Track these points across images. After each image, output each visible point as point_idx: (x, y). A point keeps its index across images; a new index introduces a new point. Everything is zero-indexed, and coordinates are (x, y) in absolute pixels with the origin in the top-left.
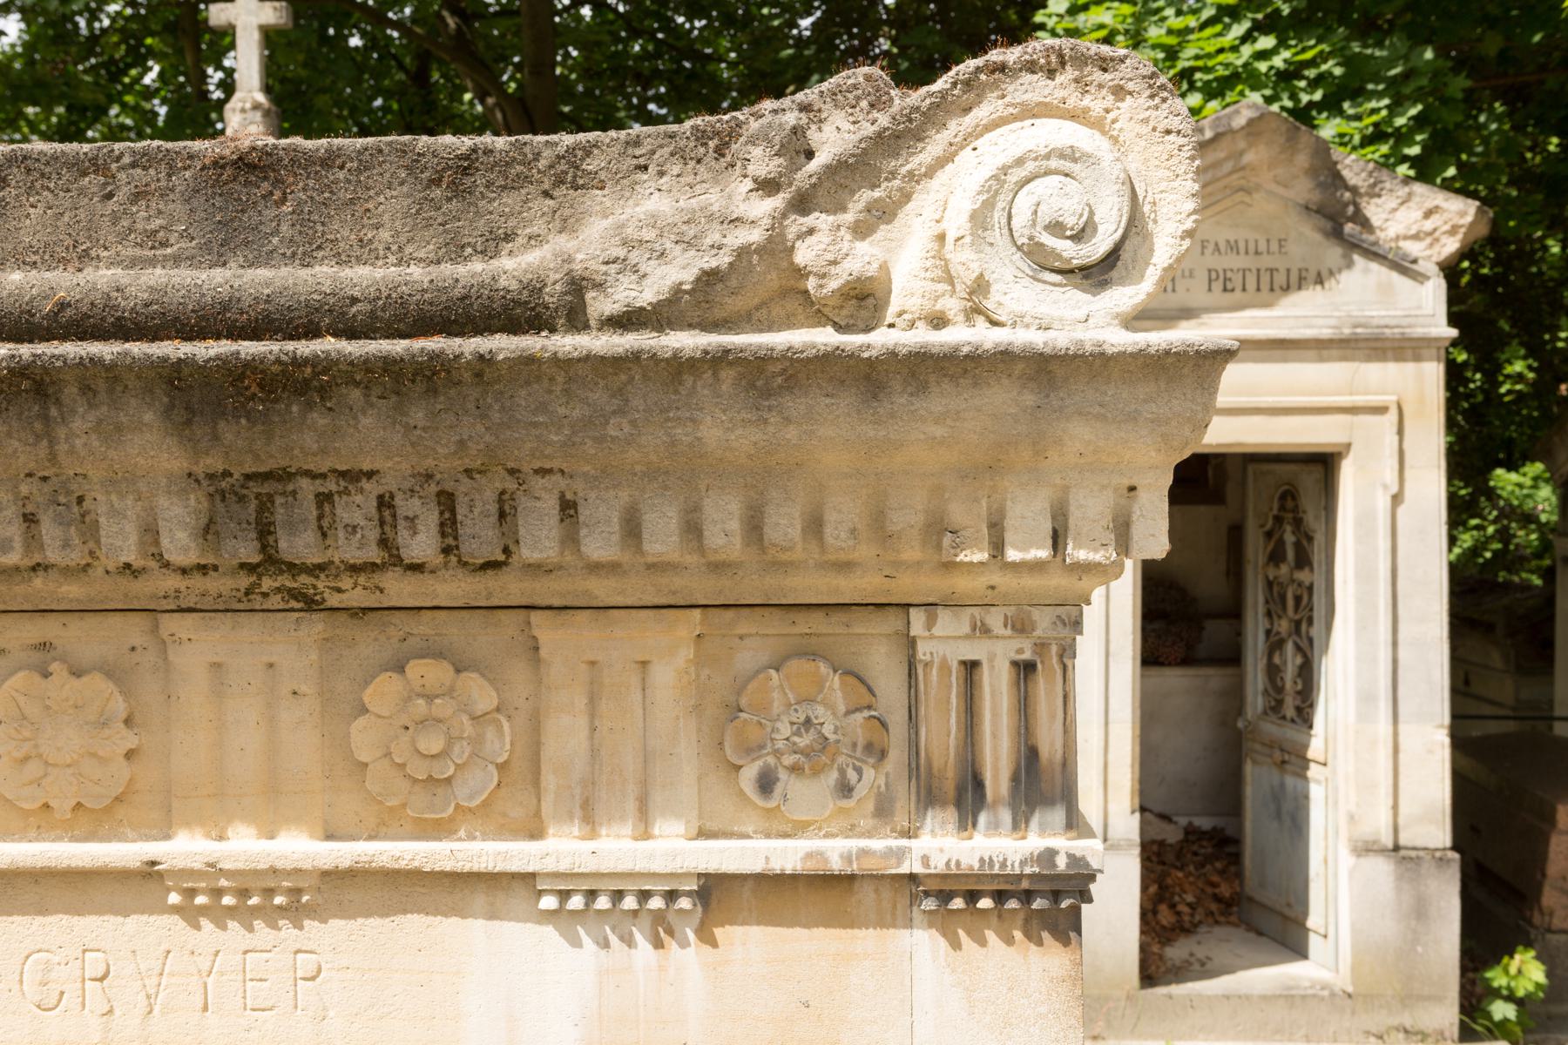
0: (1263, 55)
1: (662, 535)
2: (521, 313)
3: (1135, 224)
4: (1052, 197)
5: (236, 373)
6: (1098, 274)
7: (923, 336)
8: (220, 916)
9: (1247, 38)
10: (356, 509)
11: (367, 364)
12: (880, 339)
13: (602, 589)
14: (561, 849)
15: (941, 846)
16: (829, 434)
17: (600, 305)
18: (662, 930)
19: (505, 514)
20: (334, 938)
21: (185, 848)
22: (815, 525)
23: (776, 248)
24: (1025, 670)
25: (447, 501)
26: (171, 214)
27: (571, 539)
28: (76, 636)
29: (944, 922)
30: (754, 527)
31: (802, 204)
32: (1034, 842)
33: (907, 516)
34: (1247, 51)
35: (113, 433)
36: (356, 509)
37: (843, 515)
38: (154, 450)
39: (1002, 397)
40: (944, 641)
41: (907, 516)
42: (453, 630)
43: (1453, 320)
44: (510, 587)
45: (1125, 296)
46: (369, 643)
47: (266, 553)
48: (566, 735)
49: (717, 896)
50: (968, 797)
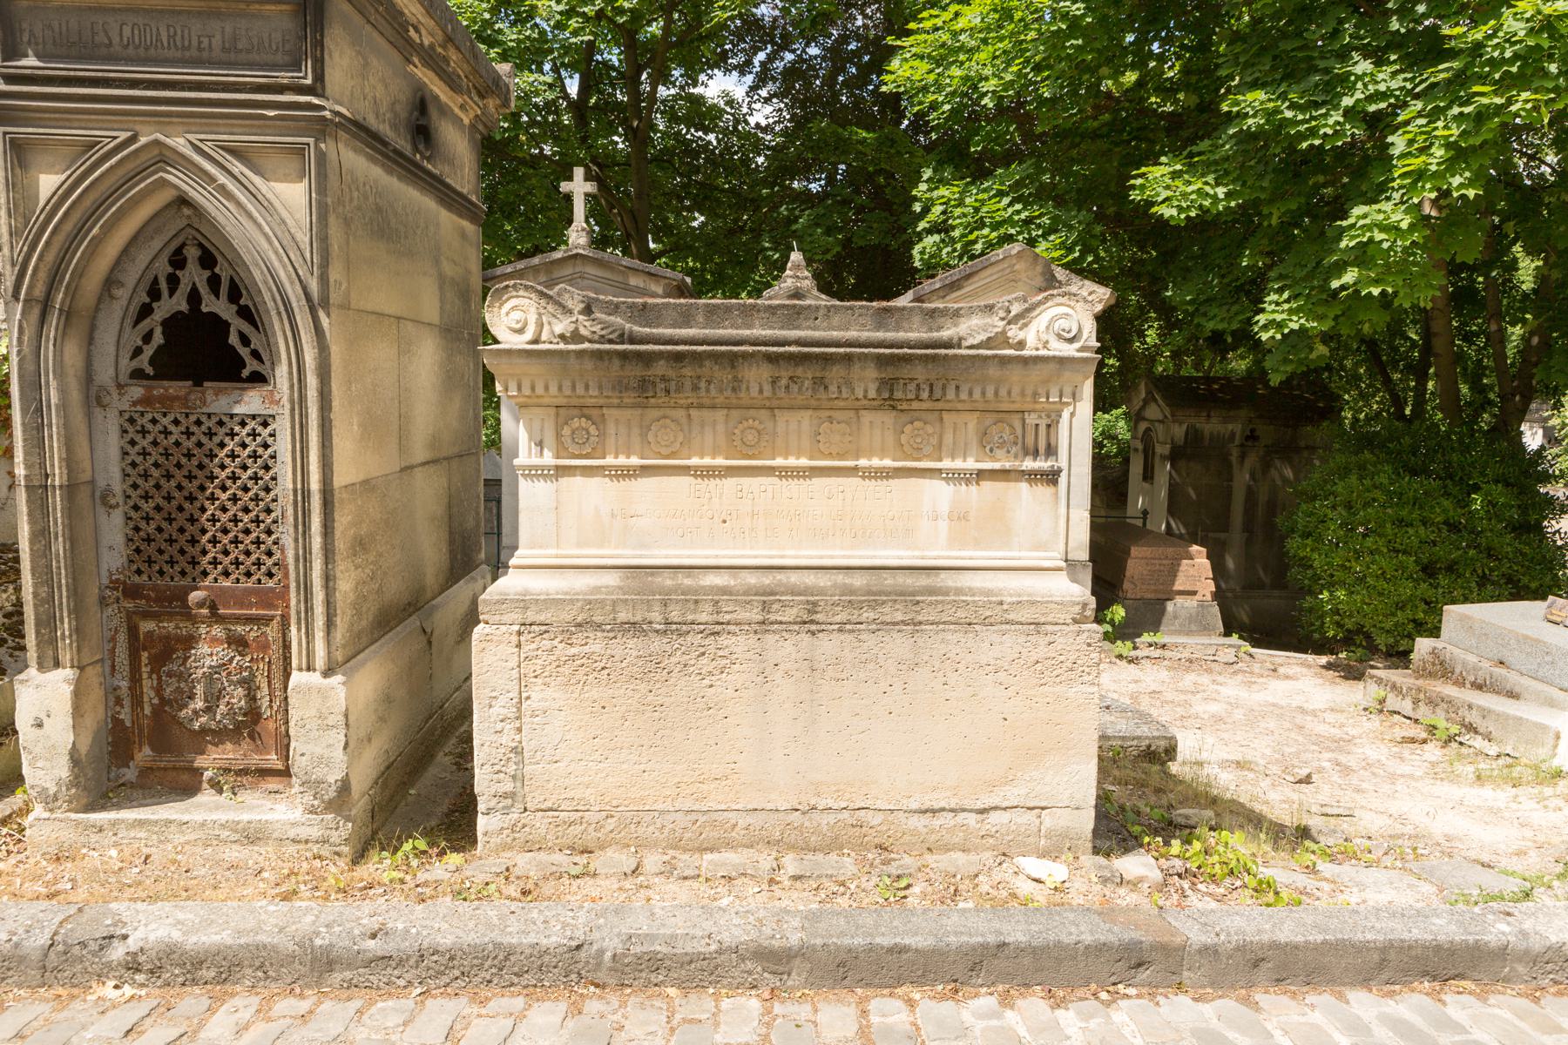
0: (1018, 212)
1: (977, 395)
2: (948, 345)
3: (1080, 330)
4: (1063, 323)
5: (892, 356)
6: (1071, 340)
7: (1034, 353)
8: (870, 478)
9: (1011, 204)
10: (912, 387)
11: (921, 356)
12: (1025, 353)
13: (959, 406)
14: (946, 464)
15: (1029, 464)
16: (1015, 374)
17: (965, 344)
18: (968, 482)
19: (944, 388)
20: (895, 483)
21: (863, 462)
22: (1009, 393)
23: (1004, 332)
24: (1049, 426)
25: (931, 386)
26: (868, 320)
27: (957, 395)
28: (837, 415)
29: (1029, 481)
30: (996, 393)
31: (1009, 323)
32: (1049, 463)
33: (1029, 392)
34: (1010, 210)
35: (863, 369)
36: (912, 387)
37: (1016, 390)
38: (871, 373)
39: (1052, 366)
40: (1031, 419)
41: (1029, 392)
42: (923, 415)
43: (1098, 340)
44: (940, 405)
45: (1077, 345)
46: (905, 418)
47: (890, 398)
48: (948, 438)
49: (981, 475)
50: (1036, 454)
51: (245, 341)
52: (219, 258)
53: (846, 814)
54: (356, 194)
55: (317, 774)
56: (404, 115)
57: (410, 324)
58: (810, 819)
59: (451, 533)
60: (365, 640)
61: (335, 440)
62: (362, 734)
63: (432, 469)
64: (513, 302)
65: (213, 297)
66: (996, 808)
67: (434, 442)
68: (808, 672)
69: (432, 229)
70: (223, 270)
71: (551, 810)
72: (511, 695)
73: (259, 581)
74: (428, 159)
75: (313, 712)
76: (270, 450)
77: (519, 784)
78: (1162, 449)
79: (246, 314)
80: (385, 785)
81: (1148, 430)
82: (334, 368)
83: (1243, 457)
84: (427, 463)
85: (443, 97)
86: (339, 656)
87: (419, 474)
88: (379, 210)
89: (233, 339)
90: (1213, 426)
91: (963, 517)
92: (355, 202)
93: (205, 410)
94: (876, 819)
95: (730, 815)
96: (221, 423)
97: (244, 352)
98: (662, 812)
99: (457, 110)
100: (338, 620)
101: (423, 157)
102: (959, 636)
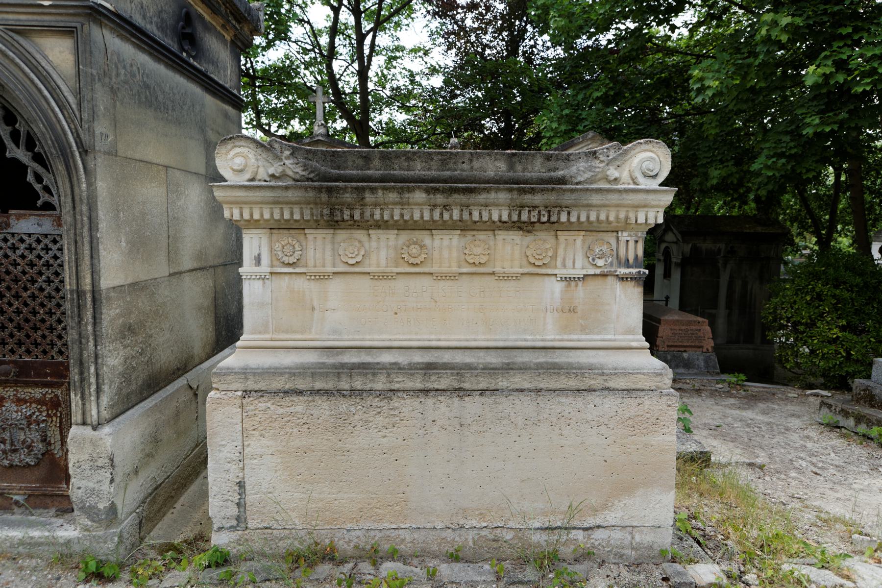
19: (559, 213)
51: (39, 179)
52: (19, 118)
53: (485, 532)
54: (123, 72)
55: (92, 501)
56: (170, 22)
57: (177, 173)
58: (460, 536)
59: (216, 317)
60: (134, 399)
61: (102, 253)
62: (129, 468)
63: (199, 274)
64: (237, 150)
65: (13, 146)
66: (599, 527)
67: (200, 255)
68: (458, 426)
69: (198, 108)
70: (20, 126)
71: (266, 528)
72: (235, 444)
73: (53, 357)
74: (194, 58)
75: (87, 457)
76: (59, 261)
77: (242, 510)
78: (676, 259)
79: (39, 158)
80: (153, 501)
81: (667, 248)
82: (100, 199)
83: (725, 265)
84: (192, 270)
85: (207, 17)
86: (105, 414)
87: (187, 278)
88: (147, 87)
89: (30, 178)
90: (706, 245)
91: (573, 310)
92: (122, 77)
93: (10, 230)
94: (509, 536)
95: (401, 532)
96: (22, 241)
97: (37, 187)
98: (348, 530)
99: (218, 28)
100: (106, 388)
101: (189, 55)
102: (571, 399)
